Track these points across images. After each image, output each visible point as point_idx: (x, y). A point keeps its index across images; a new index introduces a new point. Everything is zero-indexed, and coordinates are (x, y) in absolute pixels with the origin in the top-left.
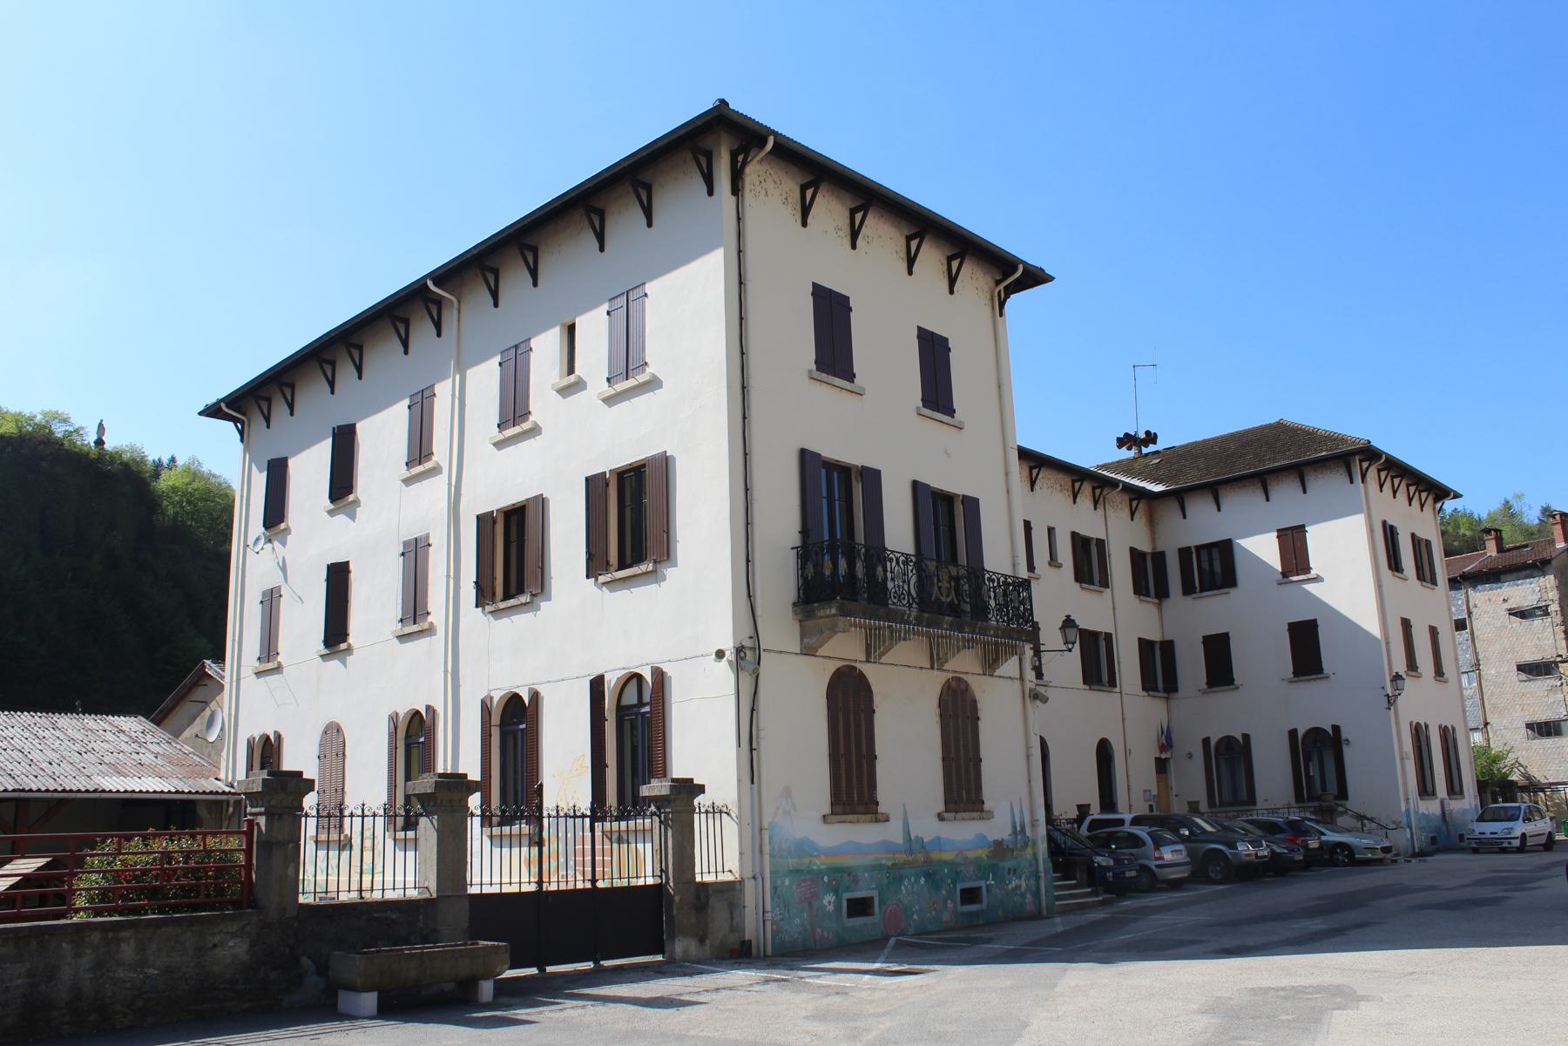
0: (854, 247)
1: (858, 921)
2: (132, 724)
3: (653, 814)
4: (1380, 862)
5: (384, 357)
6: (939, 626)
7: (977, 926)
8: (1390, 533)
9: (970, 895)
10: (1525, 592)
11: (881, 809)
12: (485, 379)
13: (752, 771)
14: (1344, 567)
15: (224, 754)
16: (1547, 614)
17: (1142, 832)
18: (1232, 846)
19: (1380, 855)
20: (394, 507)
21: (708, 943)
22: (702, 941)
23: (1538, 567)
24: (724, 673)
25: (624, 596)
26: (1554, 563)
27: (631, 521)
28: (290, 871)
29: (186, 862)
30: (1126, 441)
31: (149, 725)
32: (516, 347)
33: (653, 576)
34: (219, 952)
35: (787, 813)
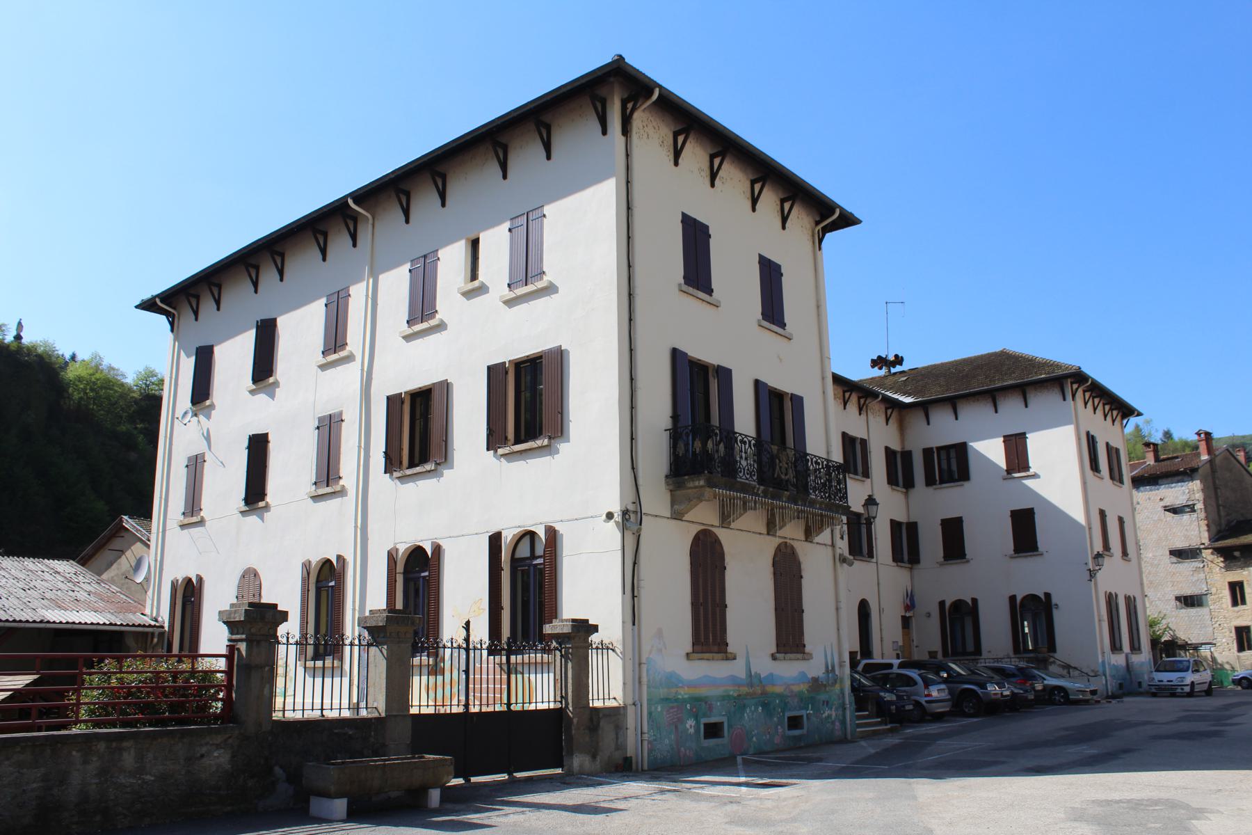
0: (713, 185)
1: (712, 742)
2: (65, 567)
3: (556, 649)
4: (1086, 702)
5: (303, 263)
6: (778, 498)
7: (800, 748)
8: (1091, 441)
9: (795, 722)
10: (1178, 493)
11: (730, 649)
12: (396, 284)
13: (633, 616)
14: (1057, 467)
15: (150, 593)
16: (1193, 510)
17: (914, 674)
18: (983, 686)
19: (1089, 697)
20: (310, 387)
21: (598, 758)
22: (594, 757)
23: (1188, 474)
24: (612, 533)
25: (519, 466)
26: (1200, 471)
27: (528, 402)
28: (266, 691)
29: (175, 681)
30: (879, 362)
31: (80, 568)
32: (425, 257)
33: (548, 450)
34: (206, 762)
35: (660, 651)
